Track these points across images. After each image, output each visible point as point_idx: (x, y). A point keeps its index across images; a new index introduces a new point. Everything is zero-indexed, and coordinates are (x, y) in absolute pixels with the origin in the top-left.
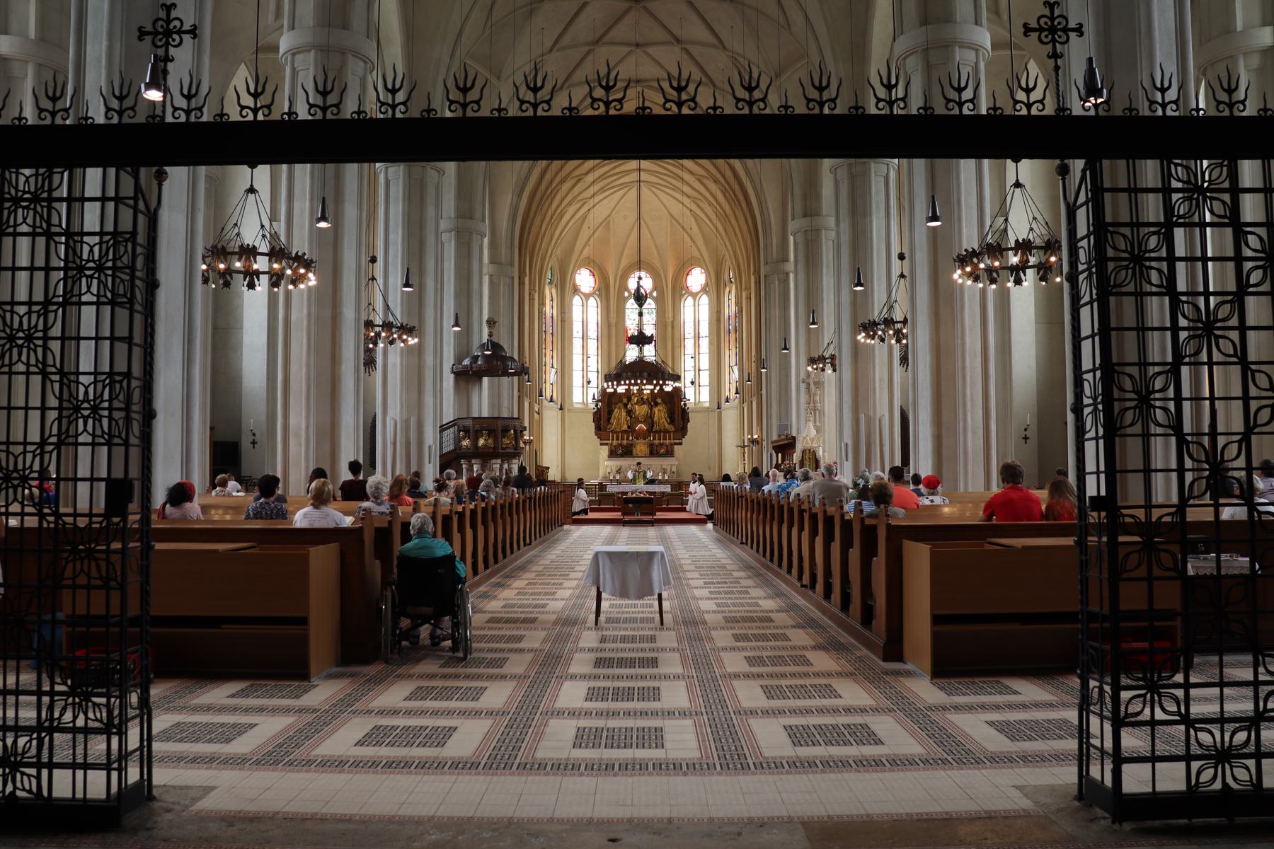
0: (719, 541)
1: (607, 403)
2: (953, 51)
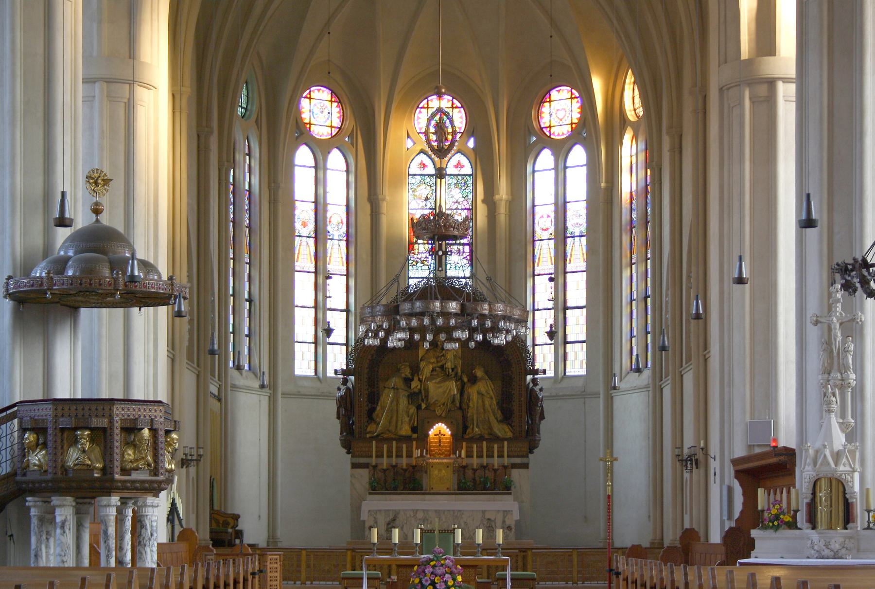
1: (368, 362)
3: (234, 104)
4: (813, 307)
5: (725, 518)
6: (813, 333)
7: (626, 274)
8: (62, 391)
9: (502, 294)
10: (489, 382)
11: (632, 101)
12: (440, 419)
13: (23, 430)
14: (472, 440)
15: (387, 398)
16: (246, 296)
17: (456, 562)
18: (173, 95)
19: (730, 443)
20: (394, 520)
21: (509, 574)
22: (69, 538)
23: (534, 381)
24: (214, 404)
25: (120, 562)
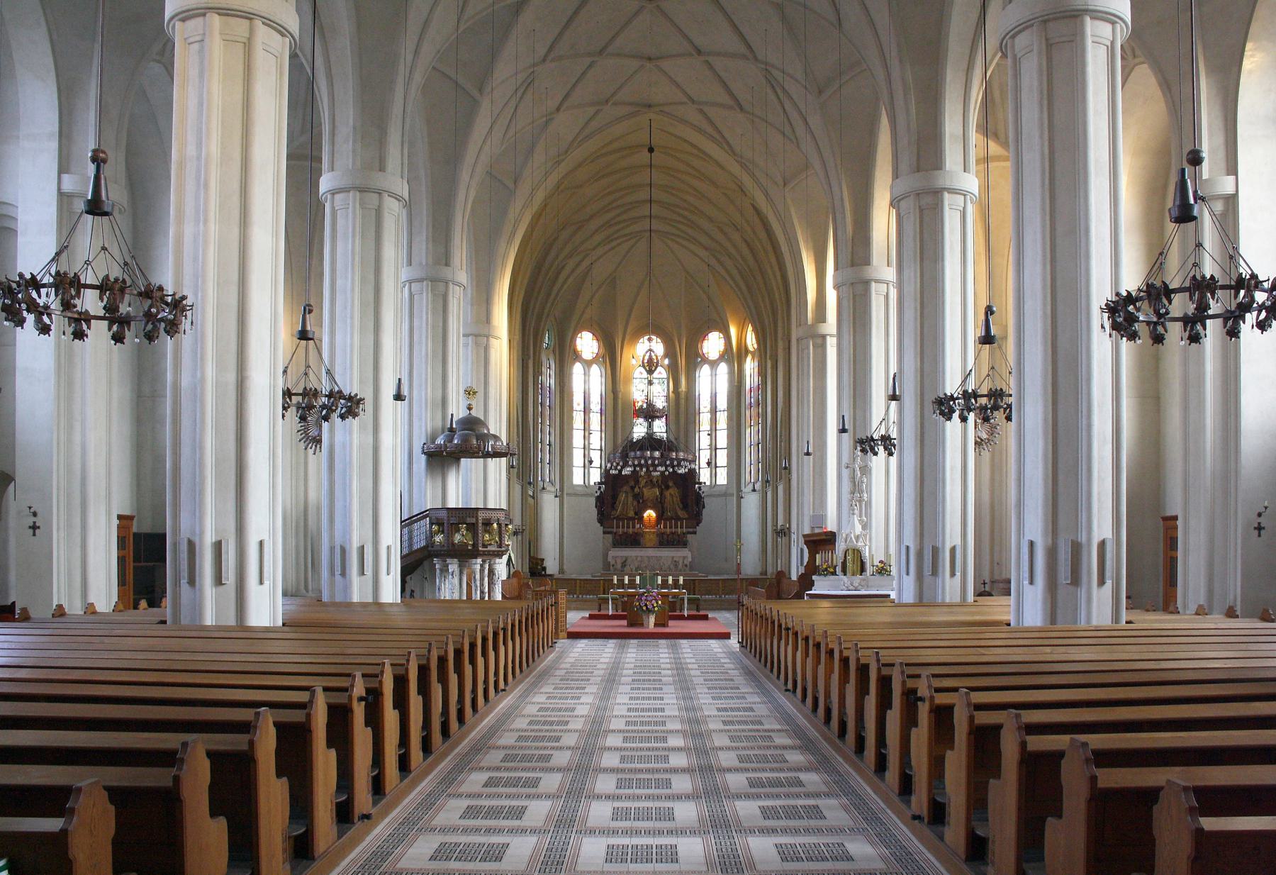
0: (748, 674)
1: (611, 482)
2: (1083, 25)
3: (542, 341)
4: (845, 460)
6: (845, 473)
7: (748, 431)
8: (452, 504)
9: (682, 446)
11: (751, 341)
12: (651, 508)
13: (431, 524)
14: (666, 520)
15: (622, 497)
17: (658, 594)
19: (802, 526)
21: (686, 597)
22: (456, 580)
24: (530, 500)
25: (482, 598)
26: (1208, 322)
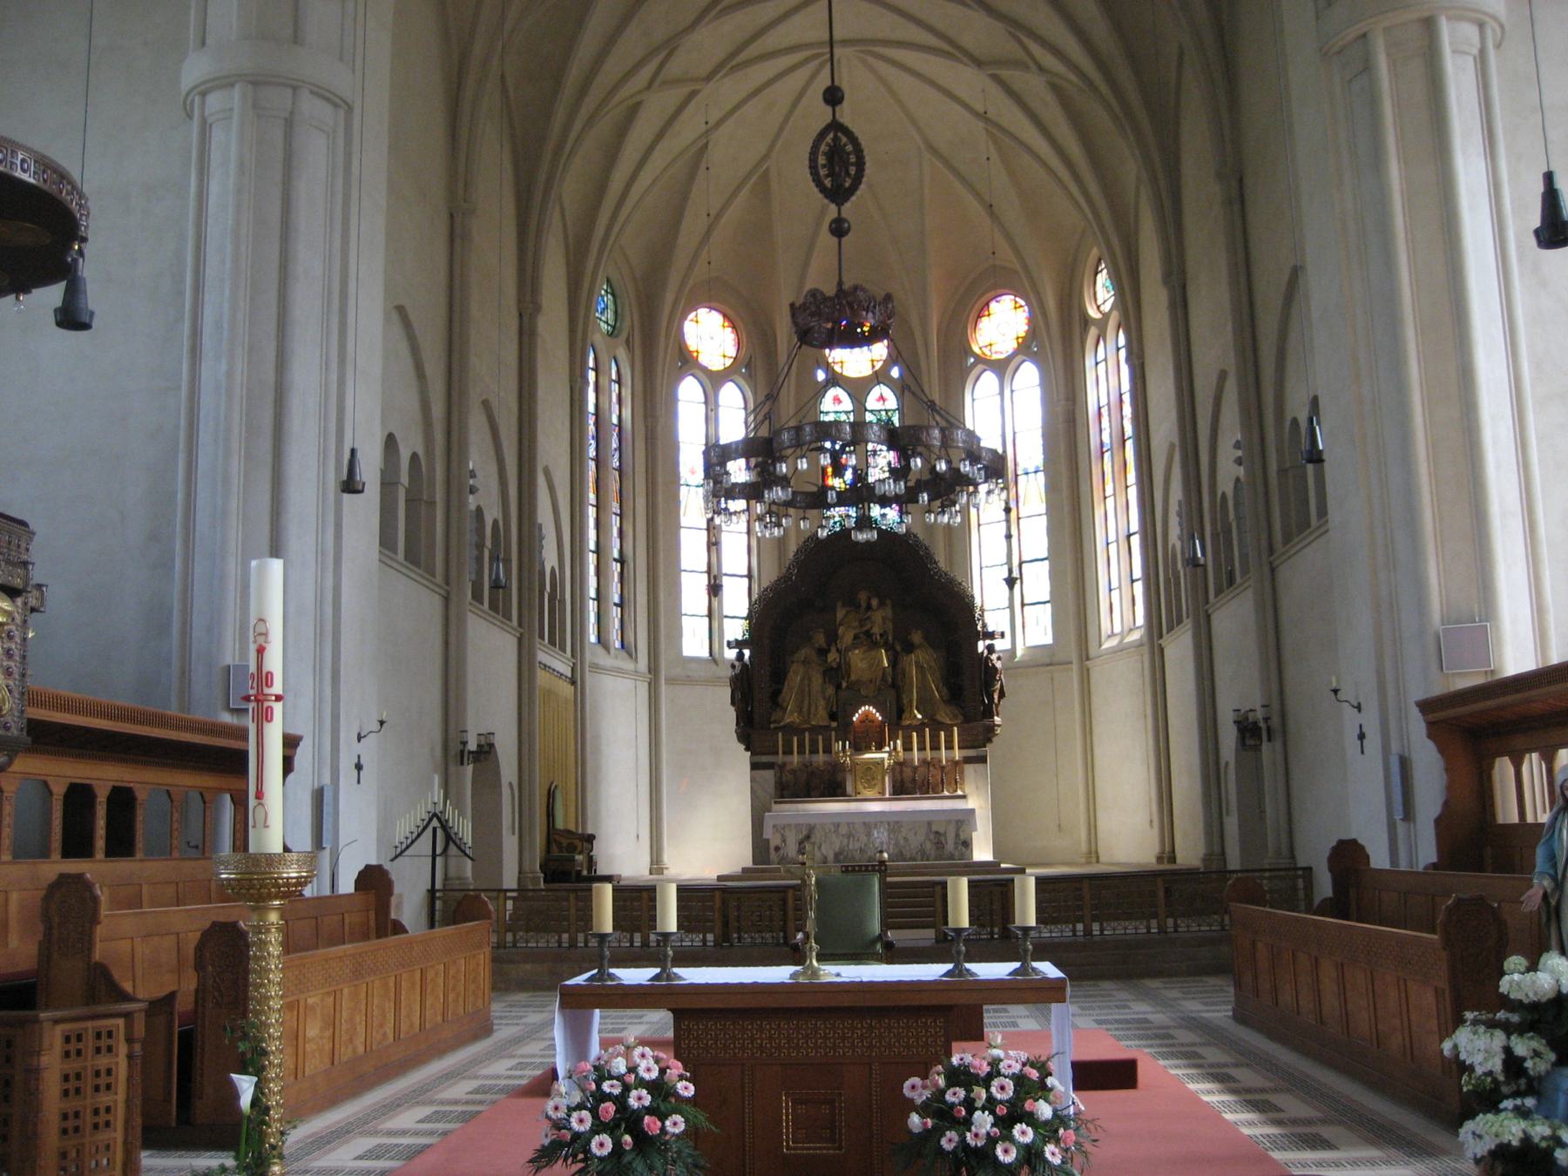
5: (1398, 817)
10: (930, 651)
15: (795, 677)
16: (616, 555)
18: (452, 216)
20: (808, 837)
23: (991, 649)
26: (515, 886)
